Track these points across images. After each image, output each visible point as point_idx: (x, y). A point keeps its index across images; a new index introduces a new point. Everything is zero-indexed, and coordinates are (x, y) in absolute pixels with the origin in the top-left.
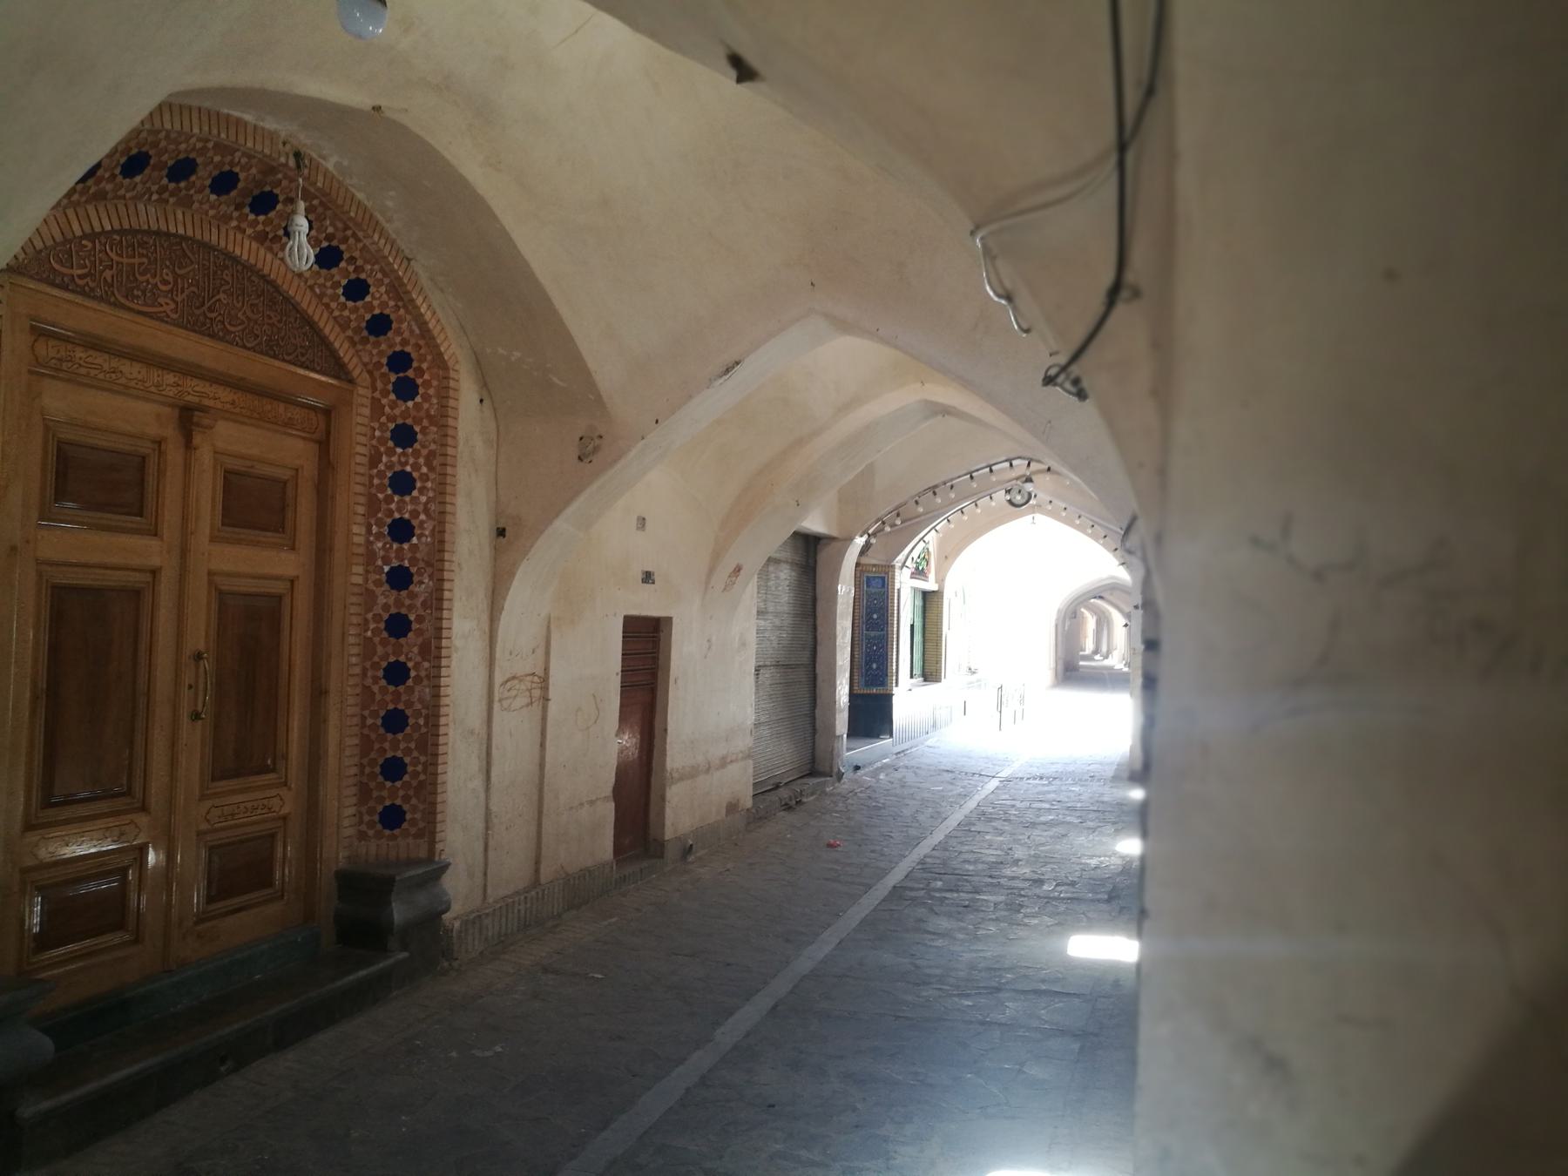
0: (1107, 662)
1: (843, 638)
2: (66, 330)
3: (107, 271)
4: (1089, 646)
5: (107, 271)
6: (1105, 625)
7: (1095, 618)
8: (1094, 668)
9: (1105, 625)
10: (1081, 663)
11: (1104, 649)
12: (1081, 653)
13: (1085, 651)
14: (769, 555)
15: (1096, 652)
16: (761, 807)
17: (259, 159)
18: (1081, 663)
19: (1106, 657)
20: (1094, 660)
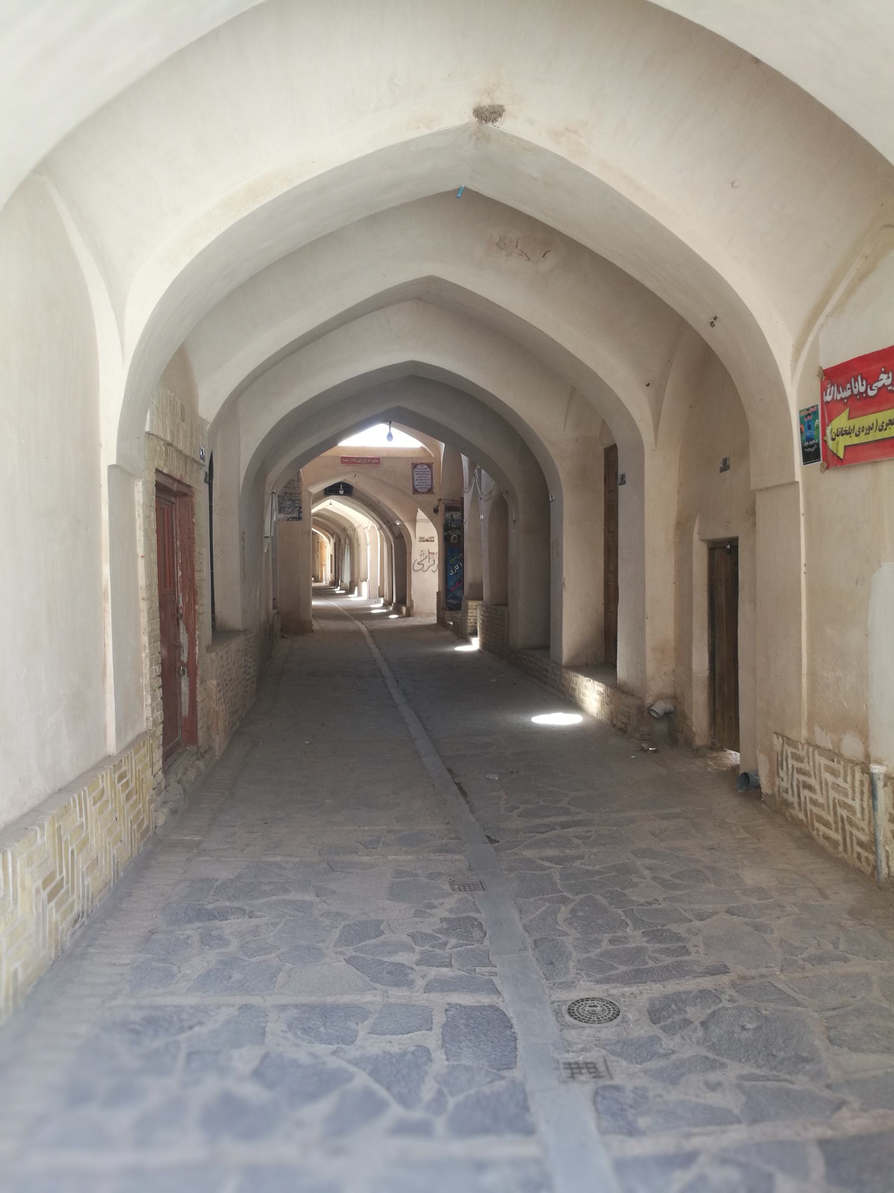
0: (354, 599)
1: (138, 837)
2: (13, 880)
3: (871, 431)
4: (327, 574)
5: (871, 431)
6: (347, 547)
7: (332, 541)
8: (483, 624)
9: (347, 547)
10: (315, 603)
11: (346, 578)
12: (314, 585)
13: (321, 581)
14: (433, 508)
15: (335, 583)
16: (459, 195)
17: (714, 1042)
18: (315, 603)
19: (350, 591)
20: (333, 595)
